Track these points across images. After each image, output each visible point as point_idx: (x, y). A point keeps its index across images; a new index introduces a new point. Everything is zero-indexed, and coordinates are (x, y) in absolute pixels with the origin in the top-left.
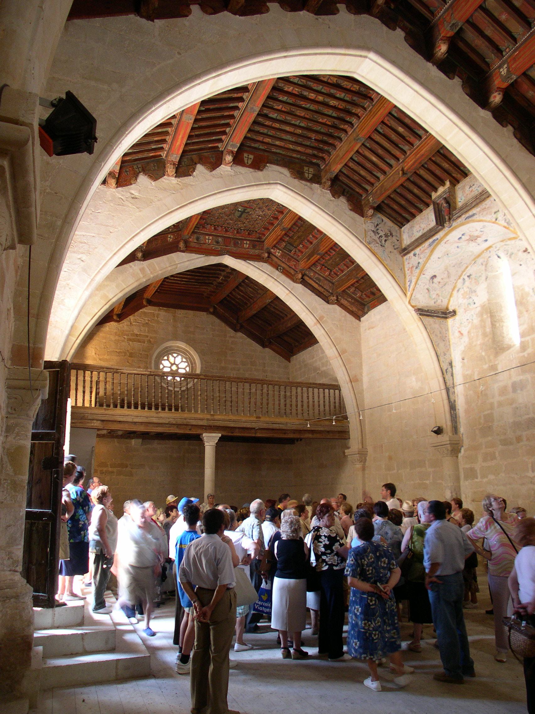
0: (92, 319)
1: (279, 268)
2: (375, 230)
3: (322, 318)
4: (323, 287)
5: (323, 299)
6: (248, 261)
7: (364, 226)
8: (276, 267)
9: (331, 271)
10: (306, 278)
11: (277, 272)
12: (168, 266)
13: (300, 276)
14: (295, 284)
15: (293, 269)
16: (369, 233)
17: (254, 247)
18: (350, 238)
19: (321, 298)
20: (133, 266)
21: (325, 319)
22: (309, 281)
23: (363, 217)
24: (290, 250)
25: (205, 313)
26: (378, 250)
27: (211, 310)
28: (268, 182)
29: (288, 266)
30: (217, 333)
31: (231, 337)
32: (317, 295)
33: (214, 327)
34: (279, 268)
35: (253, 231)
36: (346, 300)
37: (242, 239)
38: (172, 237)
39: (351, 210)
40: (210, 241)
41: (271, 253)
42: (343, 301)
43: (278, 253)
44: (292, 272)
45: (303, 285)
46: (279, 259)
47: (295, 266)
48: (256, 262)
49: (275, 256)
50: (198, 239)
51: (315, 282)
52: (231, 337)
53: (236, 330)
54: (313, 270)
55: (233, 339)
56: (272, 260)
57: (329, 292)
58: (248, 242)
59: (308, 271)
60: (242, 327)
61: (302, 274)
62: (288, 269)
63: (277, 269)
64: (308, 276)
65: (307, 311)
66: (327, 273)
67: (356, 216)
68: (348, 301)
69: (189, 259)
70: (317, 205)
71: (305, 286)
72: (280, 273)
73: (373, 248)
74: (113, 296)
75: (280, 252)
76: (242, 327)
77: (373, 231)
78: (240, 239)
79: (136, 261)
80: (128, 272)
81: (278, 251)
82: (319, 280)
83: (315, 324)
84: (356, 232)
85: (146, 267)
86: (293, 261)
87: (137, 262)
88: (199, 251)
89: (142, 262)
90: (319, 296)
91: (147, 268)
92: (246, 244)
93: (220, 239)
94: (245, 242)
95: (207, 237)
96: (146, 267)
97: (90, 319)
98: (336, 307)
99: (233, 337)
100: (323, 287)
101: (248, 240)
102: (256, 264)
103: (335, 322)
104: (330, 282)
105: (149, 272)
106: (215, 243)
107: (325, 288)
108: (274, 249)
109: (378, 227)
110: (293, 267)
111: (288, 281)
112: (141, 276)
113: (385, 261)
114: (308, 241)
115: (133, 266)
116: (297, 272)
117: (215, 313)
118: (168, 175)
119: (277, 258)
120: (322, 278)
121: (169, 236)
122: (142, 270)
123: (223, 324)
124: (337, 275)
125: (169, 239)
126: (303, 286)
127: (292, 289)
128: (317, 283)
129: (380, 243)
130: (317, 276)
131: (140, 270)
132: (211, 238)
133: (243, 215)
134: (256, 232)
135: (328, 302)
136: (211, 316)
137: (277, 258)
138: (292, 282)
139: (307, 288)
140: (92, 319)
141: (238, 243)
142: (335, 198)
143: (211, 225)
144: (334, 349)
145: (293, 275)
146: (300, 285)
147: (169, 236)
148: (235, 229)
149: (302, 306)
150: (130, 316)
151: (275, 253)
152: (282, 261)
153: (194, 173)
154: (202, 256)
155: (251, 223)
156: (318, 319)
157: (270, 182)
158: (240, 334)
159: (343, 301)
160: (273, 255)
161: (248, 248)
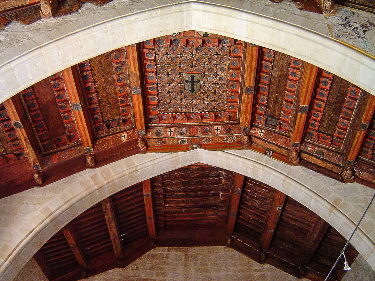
0: (27, 236)
1: (267, 151)
2: (345, 23)
3: (337, 201)
4: (329, 162)
5: (334, 178)
6: (225, 151)
7: (325, 21)
8: (264, 151)
9: (332, 136)
10: (304, 156)
11: (265, 157)
12: (125, 169)
13: (294, 154)
14: (292, 167)
15: (284, 148)
16: (335, 27)
17: (228, 132)
18: (308, 39)
19: (331, 177)
20: (83, 175)
21: (342, 202)
22: (309, 160)
23: (322, 13)
24: (274, 126)
25: (222, 247)
26: (359, 43)
27: (229, 242)
28: (178, 3)
29: (277, 145)
30: (240, 268)
31: (256, 271)
32: (325, 174)
33: (233, 262)
34: (267, 151)
35: (221, 111)
36: (366, 171)
37: (211, 125)
38: (126, 135)
39: (301, 9)
40: (172, 134)
41: (252, 135)
42: (364, 175)
43: (261, 134)
44: (284, 152)
45: (303, 166)
46: (264, 140)
47: (285, 144)
48: (236, 151)
49: (258, 138)
50: (158, 134)
51: (316, 157)
52: (256, 271)
53: (261, 262)
54: (310, 143)
55: (260, 273)
56: (257, 145)
57: (339, 166)
58: (220, 127)
59: (304, 146)
60: (267, 256)
61: (296, 151)
62: (279, 150)
63: (265, 154)
64: (306, 153)
65: (315, 196)
66: (329, 142)
67: (313, 15)
68: (369, 172)
69: (152, 159)
70: (249, 12)
71: (306, 167)
72: (271, 158)
73: (346, 40)
74: (55, 208)
75: (263, 131)
76: (267, 256)
77: (342, 25)
78: (208, 125)
79: (88, 169)
80: (76, 182)
81: (260, 131)
82: (322, 153)
83: (331, 211)
84: (314, 29)
85: (98, 173)
86: (282, 138)
87: (88, 170)
88: (162, 149)
89: (94, 169)
90: (328, 176)
91: (100, 175)
92: (218, 130)
93: (184, 129)
94: (215, 127)
95: (168, 130)
96: (98, 173)
97: (24, 236)
98: (356, 185)
99: (258, 271)
100: (329, 162)
101: (220, 125)
102: (236, 152)
103: (360, 204)
104: (337, 152)
105: (103, 179)
106: (178, 135)
107: (332, 163)
108: (255, 130)
109: (347, 20)
110: (284, 145)
111: (281, 164)
112: (92, 183)
113: (371, 53)
114: (287, 101)
115: (83, 175)
116: (290, 150)
117: (234, 246)
118: (45, 17)
119: (261, 139)
120: (324, 150)
121: (123, 135)
122: (94, 177)
123: (245, 257)
124: (342, 139)
125: (123, 138)
126: (304, 168)
127: (288, 173)
128: (319, 158)
129: (356, 35)
130: (317, 149)
131: (92, 177)
132: (172, 129)
133: (195, 87)
134: (224, 111)
135: (342, 181)
136: (230, 249)
137: (261, 139)
138: (287, 165)
139: (308, 168)
140: (27, 236)
141: (207, 130)
142: (275, 2)
143: (168, 113)
144: (365, 238)
145: (288, 157)
146: (300, 167)
147: (123, 135)
148: (197, 113)
149: (307, 191)
150: (135, 260)
151: (257, 133)
152: (267, 141)
153: (80, 11)
154: (168, 153)
155: (212, 99)
156: (332, 203)
157: (180, 3)
158: (267, 266)
159: (364, 175)
160: (255, 137)
161: (221, 134)
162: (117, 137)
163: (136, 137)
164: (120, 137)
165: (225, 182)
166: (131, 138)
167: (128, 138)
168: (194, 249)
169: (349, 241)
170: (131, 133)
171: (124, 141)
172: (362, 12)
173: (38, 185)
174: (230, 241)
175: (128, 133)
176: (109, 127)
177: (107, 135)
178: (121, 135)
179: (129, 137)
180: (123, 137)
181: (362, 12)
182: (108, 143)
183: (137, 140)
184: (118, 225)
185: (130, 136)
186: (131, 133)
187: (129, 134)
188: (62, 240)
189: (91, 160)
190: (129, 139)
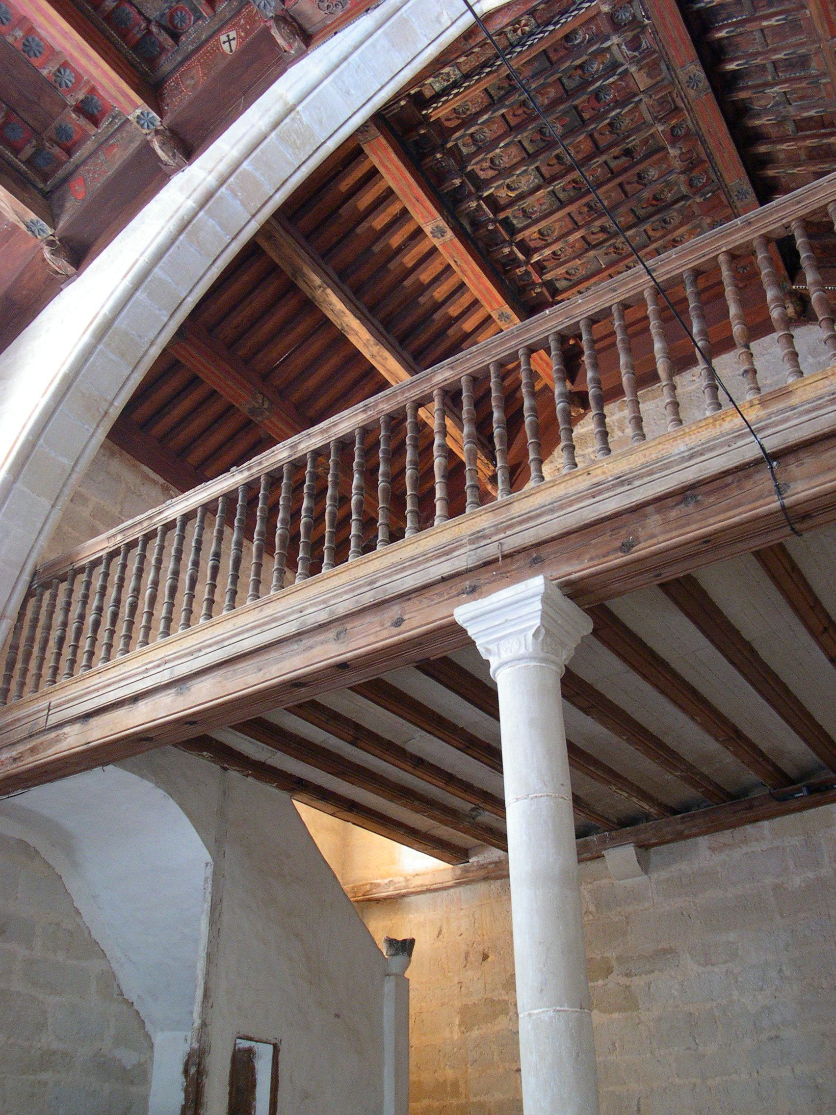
38: (233, 34)
125: (226, 47)
147: (223, 38)
162: (209, 52)
163: (262, 24)
164: (218, 49)
165: (650, 82)
166: (248, 33)
167: (241, 37)
168: (693, 376)
169: (670, 303)
170: (242, 21)
171: (231, 51)
172: (405, 178)
173: (68, 279)
174: (792, 303)
175: (234, 25)
176: (175, 36)
177: (179, 59)
178: (218, 41)
179: (243, 34)
180: (228, 36)
181: (405, 178)
182: (192, 78)
183: (267, 30)
184: (371, 309)
185: (245, 31)
186: (242, 21)
187: (241, 27)
188: (220, 418)
189: (164, 144)
190: (246, 37)
